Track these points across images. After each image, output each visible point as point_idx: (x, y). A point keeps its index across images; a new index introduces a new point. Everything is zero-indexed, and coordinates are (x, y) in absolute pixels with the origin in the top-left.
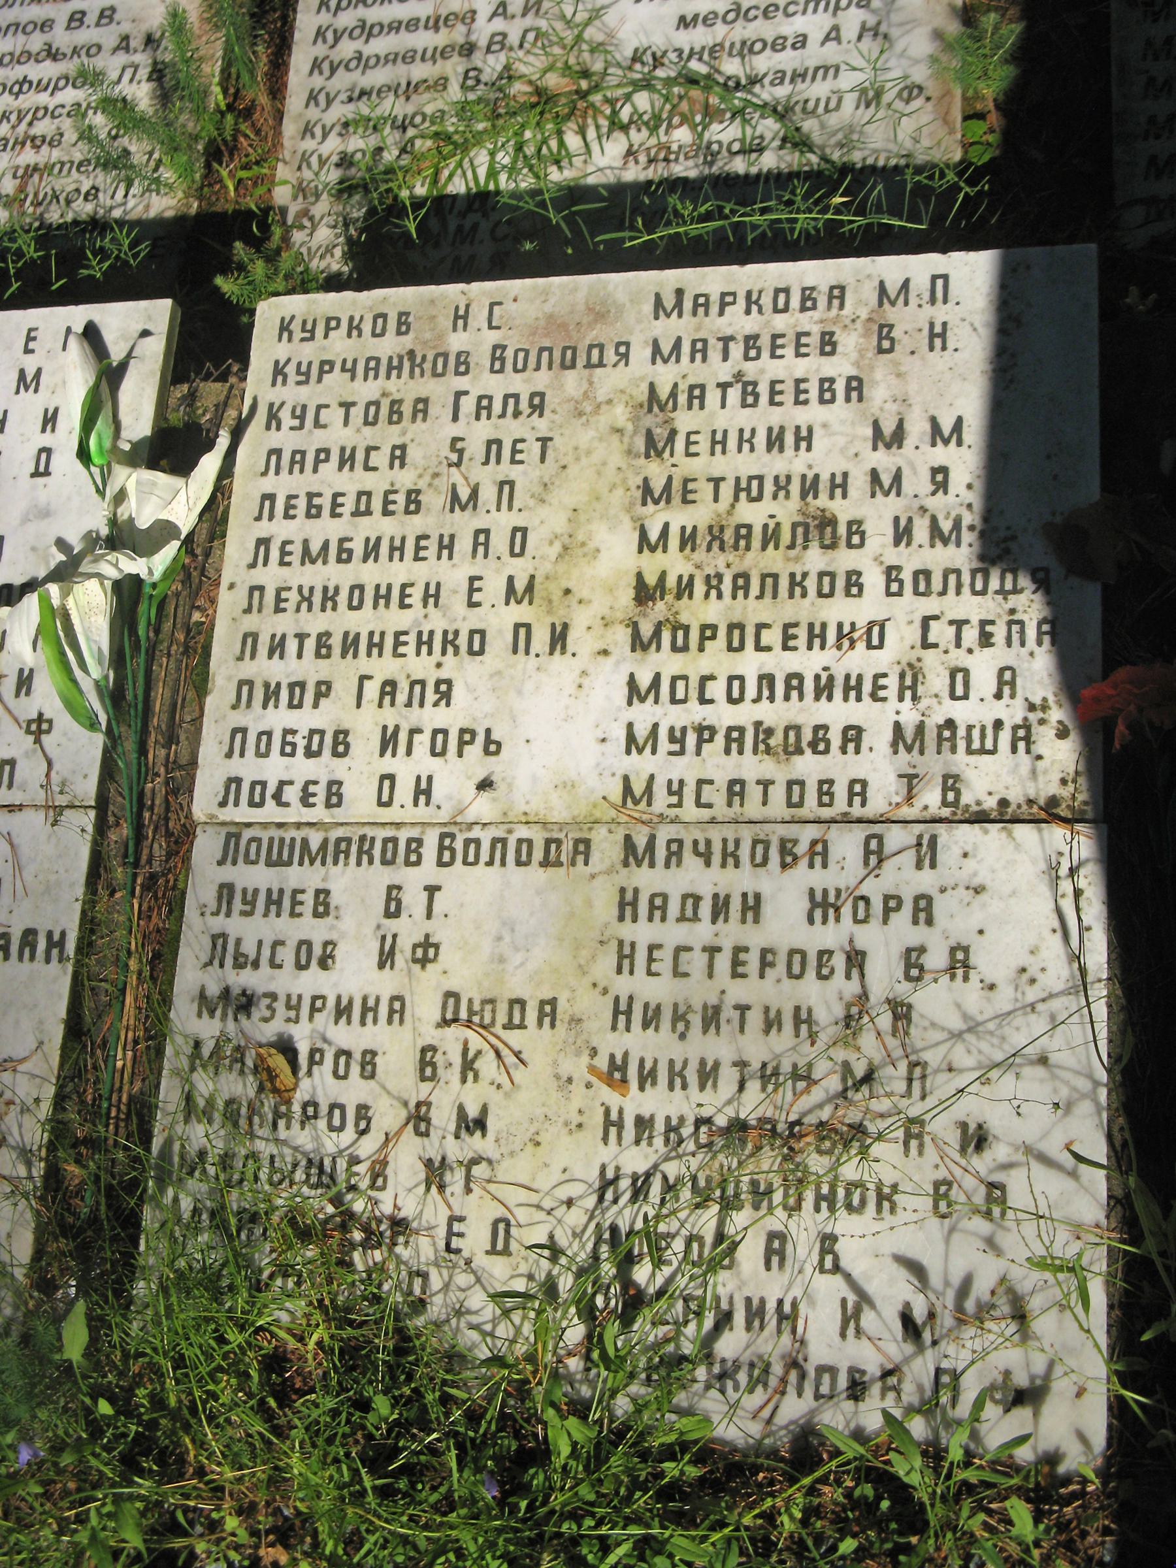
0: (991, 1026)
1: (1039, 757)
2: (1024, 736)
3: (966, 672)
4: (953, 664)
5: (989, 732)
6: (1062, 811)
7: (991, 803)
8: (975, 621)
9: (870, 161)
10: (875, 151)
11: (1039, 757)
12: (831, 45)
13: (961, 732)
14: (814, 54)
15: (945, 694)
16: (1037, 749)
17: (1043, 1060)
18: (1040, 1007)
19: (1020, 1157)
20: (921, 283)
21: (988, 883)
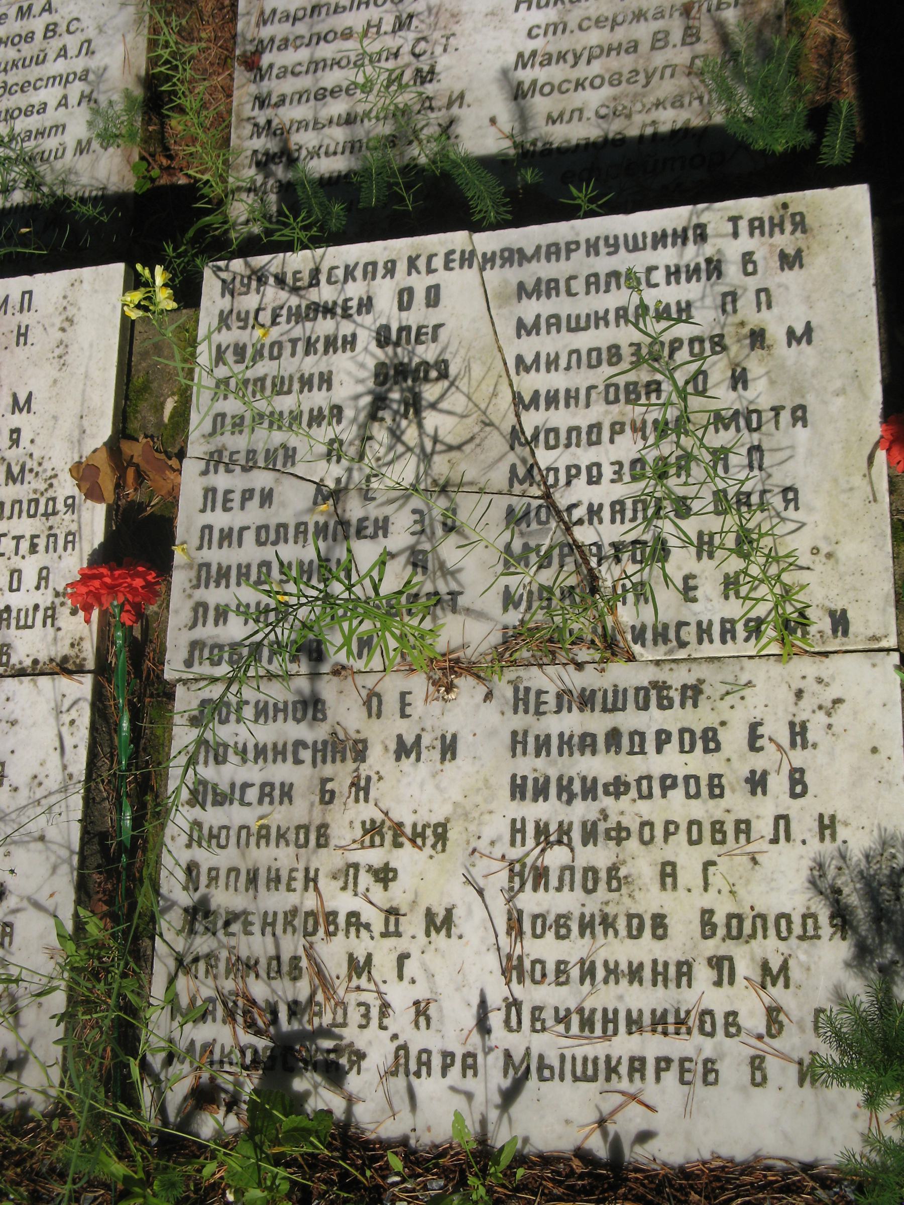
0: (13, 816)
1: (59, 629)
2: (51, 615)
3: (19, 571)
4: (13, 566)
5: (31, 613)
6: (70, 666)
7: (28, 662)
8: (28, 537)
9: (80, 194)
10: (84, 186)
11: (59, 629)
12: (62, 109)
13: (14, 614)
14: (52, 116)
15: (6, 588)
16: (60, 623)
17: (42, 838)
18: (43, 802)
19: (25, 904)
20: (15, 298)
21: (20, 718)
